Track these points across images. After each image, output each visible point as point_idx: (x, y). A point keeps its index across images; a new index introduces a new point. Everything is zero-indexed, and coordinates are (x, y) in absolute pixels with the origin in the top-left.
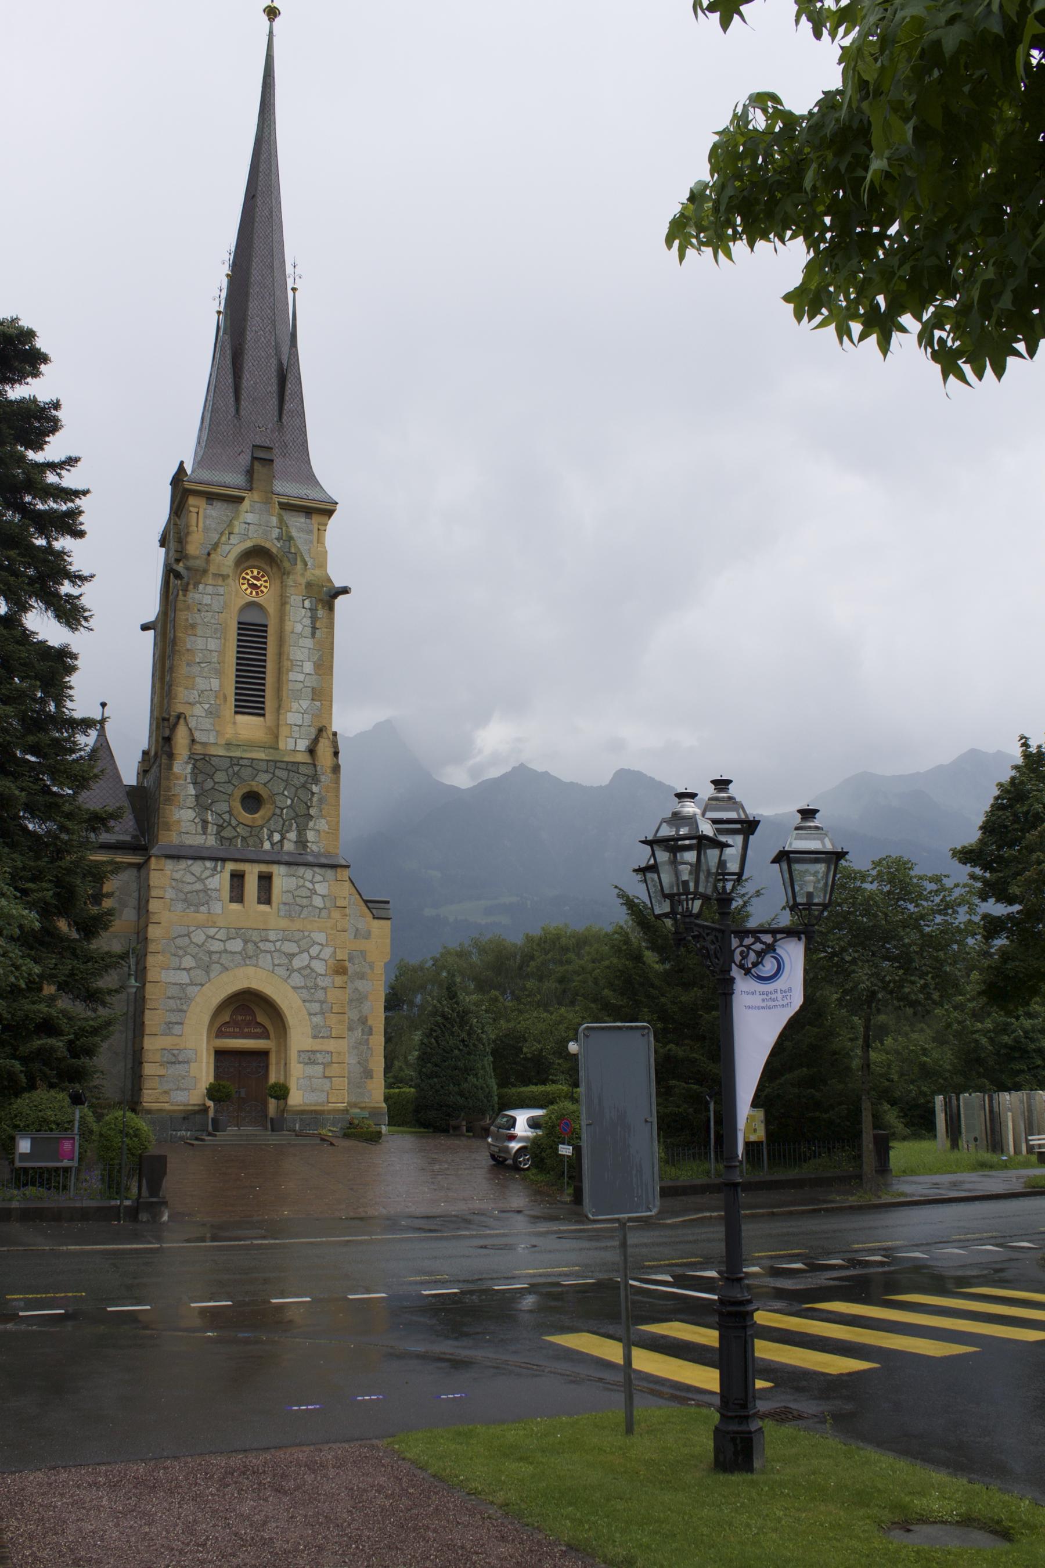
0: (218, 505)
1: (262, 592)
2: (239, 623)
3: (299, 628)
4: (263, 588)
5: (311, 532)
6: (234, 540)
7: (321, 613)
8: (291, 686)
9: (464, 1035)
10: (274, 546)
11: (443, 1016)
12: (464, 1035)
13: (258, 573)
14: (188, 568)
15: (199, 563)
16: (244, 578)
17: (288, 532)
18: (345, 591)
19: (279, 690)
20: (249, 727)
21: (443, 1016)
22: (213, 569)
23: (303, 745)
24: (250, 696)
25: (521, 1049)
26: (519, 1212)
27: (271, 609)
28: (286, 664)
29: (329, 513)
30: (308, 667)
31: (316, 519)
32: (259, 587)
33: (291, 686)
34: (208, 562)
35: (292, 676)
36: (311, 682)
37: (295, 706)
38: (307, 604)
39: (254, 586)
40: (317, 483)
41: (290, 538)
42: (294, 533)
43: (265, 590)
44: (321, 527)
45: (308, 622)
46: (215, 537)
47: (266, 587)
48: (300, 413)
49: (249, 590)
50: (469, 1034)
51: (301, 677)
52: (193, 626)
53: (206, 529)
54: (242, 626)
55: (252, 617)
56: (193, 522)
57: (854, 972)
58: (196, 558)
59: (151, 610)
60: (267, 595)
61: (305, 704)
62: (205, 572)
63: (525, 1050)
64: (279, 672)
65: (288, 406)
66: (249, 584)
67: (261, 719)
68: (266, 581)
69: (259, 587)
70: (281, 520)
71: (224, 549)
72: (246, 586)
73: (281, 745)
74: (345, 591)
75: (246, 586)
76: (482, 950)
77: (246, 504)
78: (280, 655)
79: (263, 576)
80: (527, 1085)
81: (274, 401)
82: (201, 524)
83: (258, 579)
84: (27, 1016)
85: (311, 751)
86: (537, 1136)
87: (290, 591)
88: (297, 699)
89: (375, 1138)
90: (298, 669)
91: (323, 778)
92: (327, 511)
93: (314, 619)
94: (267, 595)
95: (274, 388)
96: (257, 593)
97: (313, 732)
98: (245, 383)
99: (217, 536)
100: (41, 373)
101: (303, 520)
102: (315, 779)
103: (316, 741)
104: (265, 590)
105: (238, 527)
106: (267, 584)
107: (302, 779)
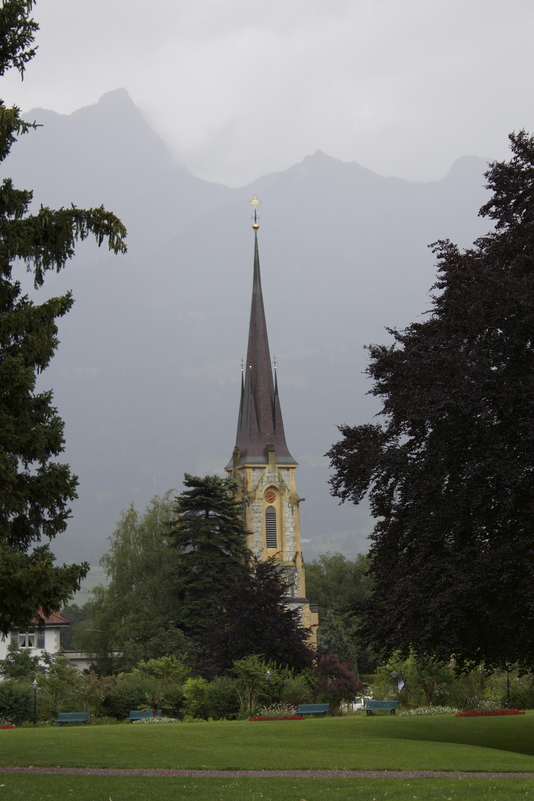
0: (256, 470)
3: (287, 515)
5: (289, 476)
6: (264, 484)
7: (295, 508)
8: (286, 537)
9: (346, 655)
10: (277, 485)
11: (338, 648)
12: (346, 655)
14: (249, 498)
15: (252, 495)
17: (282, 478)
19: (282, 539)
20: (271, 551)
21: (338, 648)
22: (257, 497)
23: (291, 559)
24: (271, 542)
25: (368, 659)
28: (284, 529)
30: (292, 529)
33: (286, 537)
34: (255, 494)
35: (286, 533)
36: (293, 535)
37: (288, 544)
38: (290, 505)
40: (290, 456)
41: (283, 481)
42: (284, 478)
45: (290, 512)
46: (257, 483)
48: (283, 432)
50: (348, 655)
51: (289, 534)
52: (252, 519)
53: (253, 481)
54: (267, 514)
56: (249, 479)
58: (251, 492)
61: (291, 543)
62: (255, 498)
63: (370, 660)
64: (282, 533)
67: (275, 549)
70: (279, 473)
71: (260, 488)
73: (284, 560)
76: (329, 565)
77: (266, 470)
78: (281, 526)
80: (371, 674)
81: (271, 421)
82: (251, 479)
84: (300, 673)
85: (294, 561)
86: (446, 291)
87: (284, 501)
88: (289, 542)
90: (288, 531)
91: (299, 571)
93: (293, 511)
95: (271, 415)
97: (294, 554)
99: (257, 483)
100: (42, 209)
101: (286, 472)
102: (296, 571)
103: (296, 557)
105: (265, 479)
107: (292, 572)
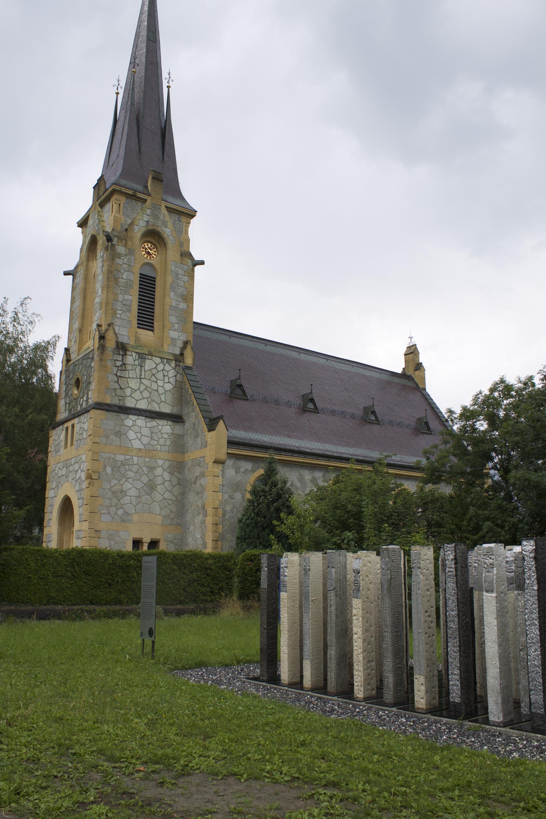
1: (153, 257)
2: (140, 274)
4: (153, 255)
13: (151, 246)
16: (143, 248)
18: (202, 263)
26: (151, 633)
27: (157, 266)
29: (193, 216)
31: (184, 219)
32: (151, 255)
39: (149, 253)
43: (155, 257)
44: (187, 225)
47: (155, 255)
49: (146, 256)
54: (142, 276)
55: (148, 272)
57: (176, 730)
59: (73, 259)
60: (155, 259)
65: (167, 147)
66: (146, 252)
68: (155, 251)
69: (151, 255)
72: (144, 253)
74: (202, 263)
75: (144, 253)
79: (153, 248)
83: (151, 250)
89: (205, 520)
92: (191, 214)
94: (155, 259)
96: (150, 258)
98: (117, 126)
104: (155, 257)
106: (156, 253)
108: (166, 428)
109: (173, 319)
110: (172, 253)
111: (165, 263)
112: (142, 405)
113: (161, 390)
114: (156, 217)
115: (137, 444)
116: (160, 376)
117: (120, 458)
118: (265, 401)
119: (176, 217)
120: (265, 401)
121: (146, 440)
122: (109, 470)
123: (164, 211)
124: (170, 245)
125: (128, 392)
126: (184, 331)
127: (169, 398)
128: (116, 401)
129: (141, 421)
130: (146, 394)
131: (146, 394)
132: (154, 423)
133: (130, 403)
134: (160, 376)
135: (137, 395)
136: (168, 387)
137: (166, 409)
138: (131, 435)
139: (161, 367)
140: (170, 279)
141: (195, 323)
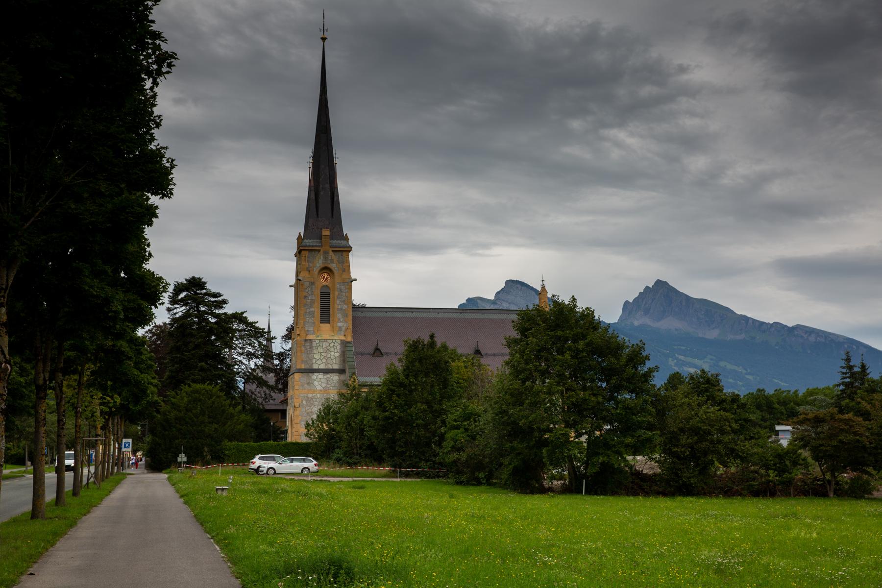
18: (355, 280)
31: (344, 254)
74: (355, 280)
108: (335, 377)
109: (339, 316)
110: (338, 279)
111: (334, 283)
112: (322, 367)
113: (333, 357)
114: (326, 258)
115: (319, 388)
116: (332, 349)
117: (310, 395)
118: (362, 354)
119: (340, 254)
120: (362, 354)
121: (324, 385)
122: (304, 402)
123: (331, 253)
124: (335, 271)
125: (314, 361)
126: (346, 322)
127: (338, 360)
128: (307, 367)
129: (321, 376)
130: (324, 361)
131: (324, 361)
132: (328, 376)
133: (315, 367)
134: (332, 349)
135: (319, 362)
136: (337, 355)
137: (336, 367)
138: (316, 383)
139: (332, 345)
140: (337, 293)
141: (356, 308)
